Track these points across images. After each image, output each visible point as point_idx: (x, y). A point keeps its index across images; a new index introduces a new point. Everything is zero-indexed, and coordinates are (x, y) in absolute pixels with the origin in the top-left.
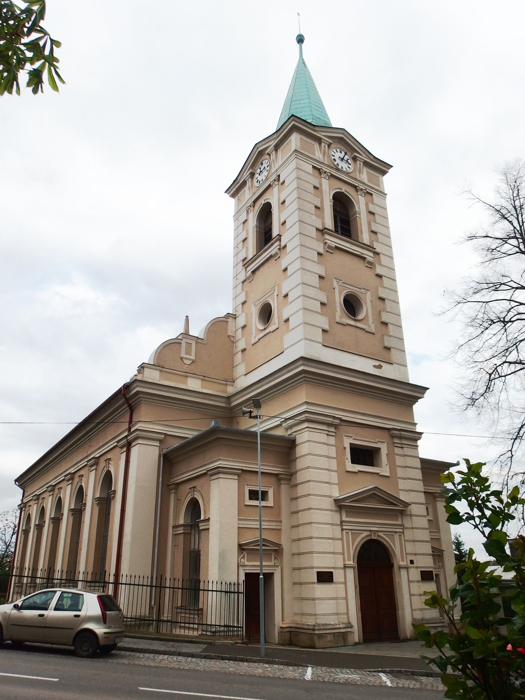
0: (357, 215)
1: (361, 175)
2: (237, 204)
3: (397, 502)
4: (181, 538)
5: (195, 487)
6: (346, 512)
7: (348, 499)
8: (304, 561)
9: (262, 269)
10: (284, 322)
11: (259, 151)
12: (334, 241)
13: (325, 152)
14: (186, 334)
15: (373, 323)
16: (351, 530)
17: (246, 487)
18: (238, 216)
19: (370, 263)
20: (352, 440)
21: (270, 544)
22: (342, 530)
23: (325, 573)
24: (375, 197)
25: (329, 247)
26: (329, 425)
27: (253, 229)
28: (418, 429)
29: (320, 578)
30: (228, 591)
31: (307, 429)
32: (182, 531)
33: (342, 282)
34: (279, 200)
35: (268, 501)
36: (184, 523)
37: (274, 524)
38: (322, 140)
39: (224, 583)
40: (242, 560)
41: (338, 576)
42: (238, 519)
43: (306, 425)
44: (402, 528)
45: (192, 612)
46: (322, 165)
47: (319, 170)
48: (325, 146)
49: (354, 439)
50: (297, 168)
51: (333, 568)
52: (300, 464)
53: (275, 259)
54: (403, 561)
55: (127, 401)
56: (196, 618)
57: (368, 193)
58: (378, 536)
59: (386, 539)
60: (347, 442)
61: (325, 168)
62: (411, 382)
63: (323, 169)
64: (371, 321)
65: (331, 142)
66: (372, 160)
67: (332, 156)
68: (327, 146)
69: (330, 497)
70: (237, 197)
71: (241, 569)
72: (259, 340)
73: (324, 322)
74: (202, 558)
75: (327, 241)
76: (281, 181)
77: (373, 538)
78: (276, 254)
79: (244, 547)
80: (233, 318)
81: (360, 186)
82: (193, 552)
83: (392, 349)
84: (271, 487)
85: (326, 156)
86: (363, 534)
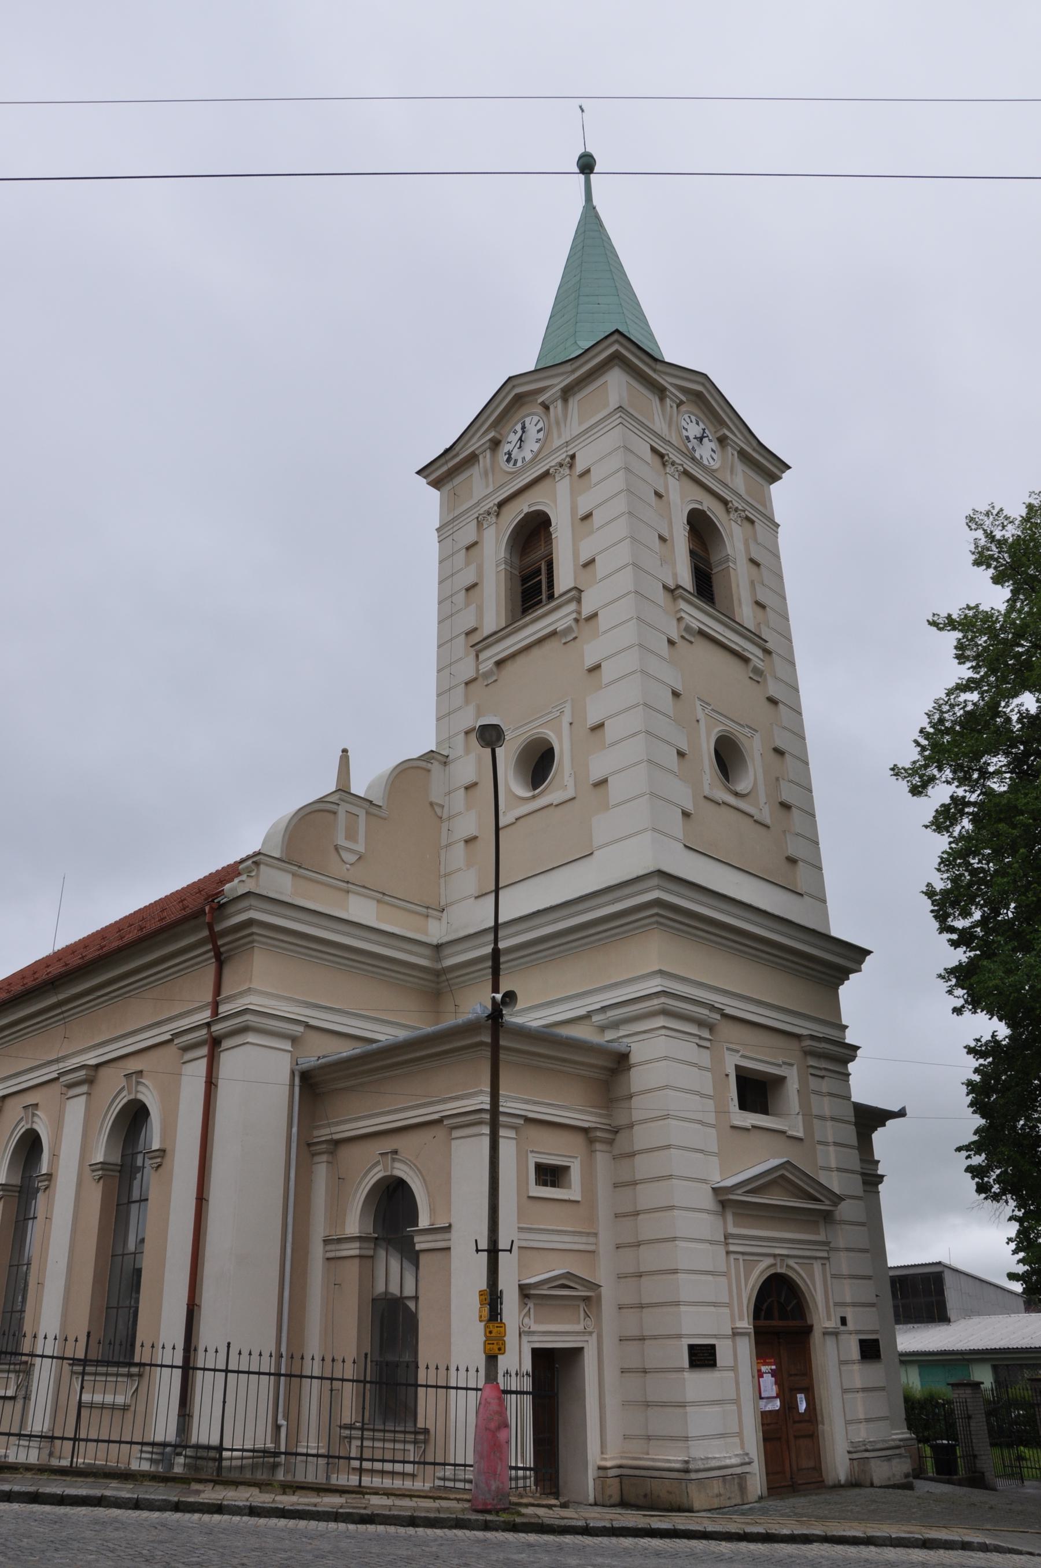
0: (731, 564)
1: (734, 477)
2: (448, 505)
3: (822, 1194)
4: (354, 1267)
5: (395, 1152)
6: (734, 1214)
7: (738, 1189)
8: (653, 1322)
9: (521, 660)
10: (592, 786)
11: (516, 394)
12: (697, 616)
13: (671, 418)
14: (343, 789)
15: (766, 803)
16: (743, 1253)
17: (530, 1155)
18: (455, 529)
19: (757, 671)
20: (740, 1059)
21: (576, 1283)
22: (728, 1253)
23: (703, 1348)
24: (758, 525)
25: (688, 629)
26: (701, 1023)
27: (497, 566)
28: (850, 1038)
29: (694, 1358)
30: (525, 1396)
31: (663, 1032)
32: (356, 1252)
33: (710, 708)
34: (574, 509)
35: (569, 1187)
36: (360, 1233)
37: (584, 1239)
38: (668, 393)
39: (245, 1353)
40: (526, 1320)
41: (723, 1356)
42: (519, 1228)
43: (660, 1021)
44: (827, 1248)
45: (401, 1436)
46: (668, 448)
47: (662, 456)
48: (671, 407)
49: (742, 1056)
50: (625, 447)
51: (715, 1336)
52: (641, 1108)
53: (564, 641)
54: (829, 1319)
55: (213, 937)
56: (11, 1378)
57: (748, 519)
58: (788, 1266)
59: (798, 1272)
60: (730, 1062)
61: (674, 456)
62: (835, 933)
63: (671, 455)
64: (762, 799)
65: (684, 399)
66: (754, 450)
67: (683, 430)
68: (675, 406)
69: (704, 1181)
70: (449, 486)
71: (525, 1339)
72: (516, 819)
73: (684, 797)
74: (710, 1369)
75: (683, 615)
76: (580, 466)
77: (779, 1271)
78: (568, 630)
79: (532, 1292)
80: (440, 762)
81: (734, 502)
82: (384, 1299)
83: (800, 863)
84: (576, 1157)
85: (674, 428)
86: (761, 1263)
